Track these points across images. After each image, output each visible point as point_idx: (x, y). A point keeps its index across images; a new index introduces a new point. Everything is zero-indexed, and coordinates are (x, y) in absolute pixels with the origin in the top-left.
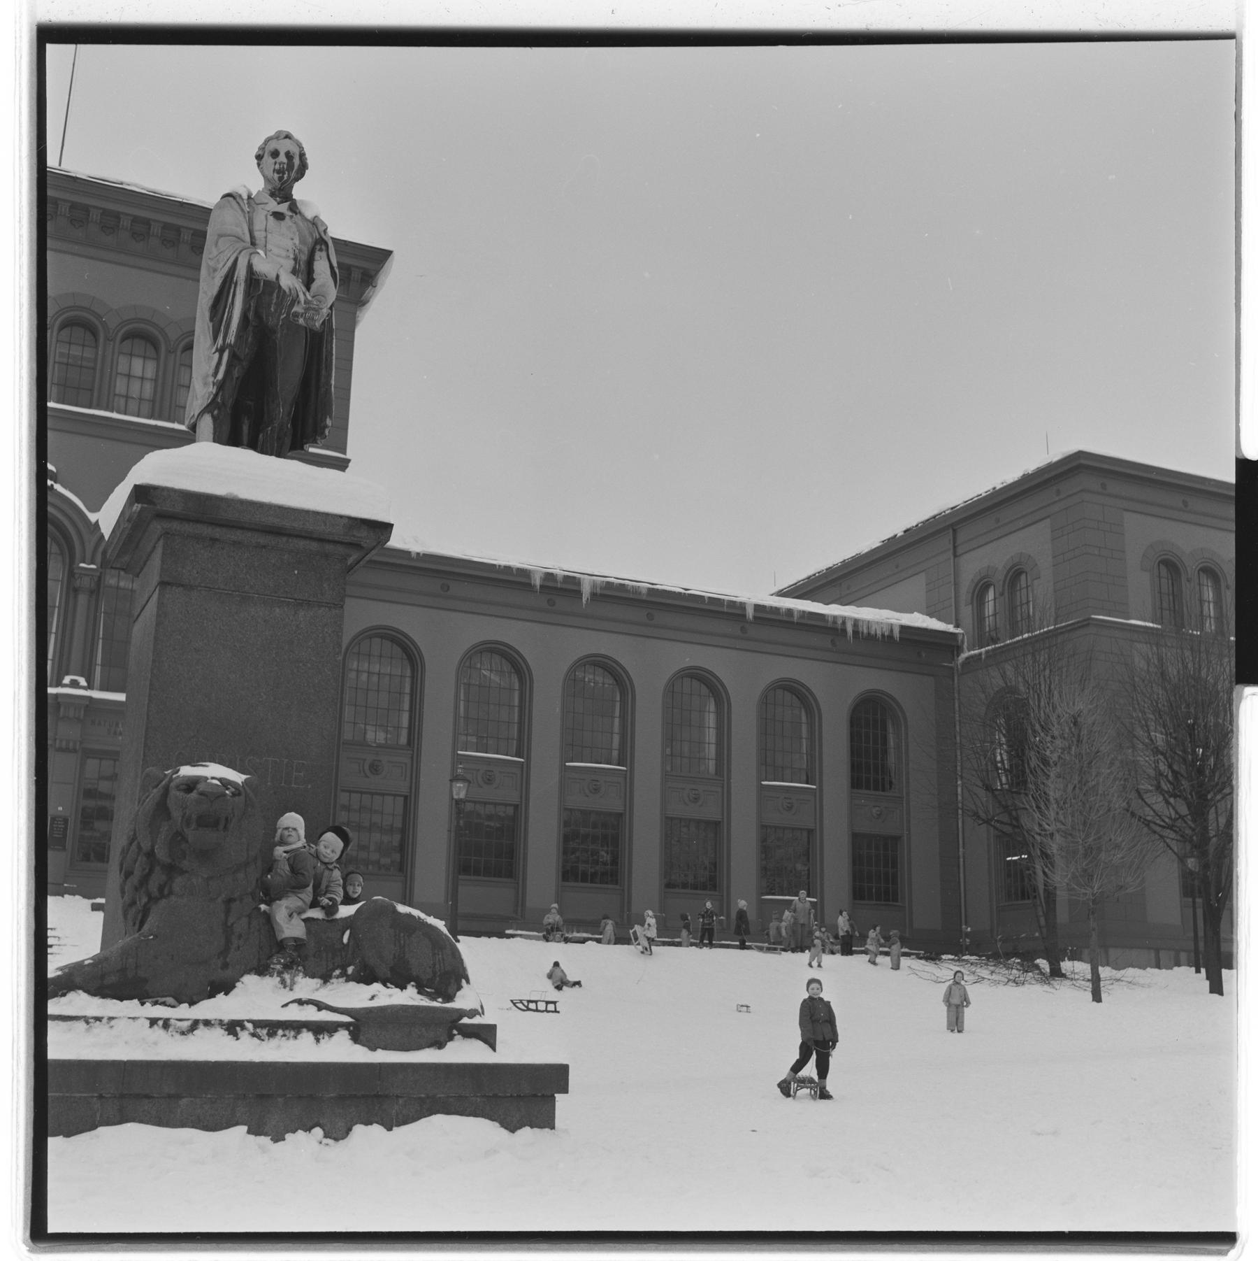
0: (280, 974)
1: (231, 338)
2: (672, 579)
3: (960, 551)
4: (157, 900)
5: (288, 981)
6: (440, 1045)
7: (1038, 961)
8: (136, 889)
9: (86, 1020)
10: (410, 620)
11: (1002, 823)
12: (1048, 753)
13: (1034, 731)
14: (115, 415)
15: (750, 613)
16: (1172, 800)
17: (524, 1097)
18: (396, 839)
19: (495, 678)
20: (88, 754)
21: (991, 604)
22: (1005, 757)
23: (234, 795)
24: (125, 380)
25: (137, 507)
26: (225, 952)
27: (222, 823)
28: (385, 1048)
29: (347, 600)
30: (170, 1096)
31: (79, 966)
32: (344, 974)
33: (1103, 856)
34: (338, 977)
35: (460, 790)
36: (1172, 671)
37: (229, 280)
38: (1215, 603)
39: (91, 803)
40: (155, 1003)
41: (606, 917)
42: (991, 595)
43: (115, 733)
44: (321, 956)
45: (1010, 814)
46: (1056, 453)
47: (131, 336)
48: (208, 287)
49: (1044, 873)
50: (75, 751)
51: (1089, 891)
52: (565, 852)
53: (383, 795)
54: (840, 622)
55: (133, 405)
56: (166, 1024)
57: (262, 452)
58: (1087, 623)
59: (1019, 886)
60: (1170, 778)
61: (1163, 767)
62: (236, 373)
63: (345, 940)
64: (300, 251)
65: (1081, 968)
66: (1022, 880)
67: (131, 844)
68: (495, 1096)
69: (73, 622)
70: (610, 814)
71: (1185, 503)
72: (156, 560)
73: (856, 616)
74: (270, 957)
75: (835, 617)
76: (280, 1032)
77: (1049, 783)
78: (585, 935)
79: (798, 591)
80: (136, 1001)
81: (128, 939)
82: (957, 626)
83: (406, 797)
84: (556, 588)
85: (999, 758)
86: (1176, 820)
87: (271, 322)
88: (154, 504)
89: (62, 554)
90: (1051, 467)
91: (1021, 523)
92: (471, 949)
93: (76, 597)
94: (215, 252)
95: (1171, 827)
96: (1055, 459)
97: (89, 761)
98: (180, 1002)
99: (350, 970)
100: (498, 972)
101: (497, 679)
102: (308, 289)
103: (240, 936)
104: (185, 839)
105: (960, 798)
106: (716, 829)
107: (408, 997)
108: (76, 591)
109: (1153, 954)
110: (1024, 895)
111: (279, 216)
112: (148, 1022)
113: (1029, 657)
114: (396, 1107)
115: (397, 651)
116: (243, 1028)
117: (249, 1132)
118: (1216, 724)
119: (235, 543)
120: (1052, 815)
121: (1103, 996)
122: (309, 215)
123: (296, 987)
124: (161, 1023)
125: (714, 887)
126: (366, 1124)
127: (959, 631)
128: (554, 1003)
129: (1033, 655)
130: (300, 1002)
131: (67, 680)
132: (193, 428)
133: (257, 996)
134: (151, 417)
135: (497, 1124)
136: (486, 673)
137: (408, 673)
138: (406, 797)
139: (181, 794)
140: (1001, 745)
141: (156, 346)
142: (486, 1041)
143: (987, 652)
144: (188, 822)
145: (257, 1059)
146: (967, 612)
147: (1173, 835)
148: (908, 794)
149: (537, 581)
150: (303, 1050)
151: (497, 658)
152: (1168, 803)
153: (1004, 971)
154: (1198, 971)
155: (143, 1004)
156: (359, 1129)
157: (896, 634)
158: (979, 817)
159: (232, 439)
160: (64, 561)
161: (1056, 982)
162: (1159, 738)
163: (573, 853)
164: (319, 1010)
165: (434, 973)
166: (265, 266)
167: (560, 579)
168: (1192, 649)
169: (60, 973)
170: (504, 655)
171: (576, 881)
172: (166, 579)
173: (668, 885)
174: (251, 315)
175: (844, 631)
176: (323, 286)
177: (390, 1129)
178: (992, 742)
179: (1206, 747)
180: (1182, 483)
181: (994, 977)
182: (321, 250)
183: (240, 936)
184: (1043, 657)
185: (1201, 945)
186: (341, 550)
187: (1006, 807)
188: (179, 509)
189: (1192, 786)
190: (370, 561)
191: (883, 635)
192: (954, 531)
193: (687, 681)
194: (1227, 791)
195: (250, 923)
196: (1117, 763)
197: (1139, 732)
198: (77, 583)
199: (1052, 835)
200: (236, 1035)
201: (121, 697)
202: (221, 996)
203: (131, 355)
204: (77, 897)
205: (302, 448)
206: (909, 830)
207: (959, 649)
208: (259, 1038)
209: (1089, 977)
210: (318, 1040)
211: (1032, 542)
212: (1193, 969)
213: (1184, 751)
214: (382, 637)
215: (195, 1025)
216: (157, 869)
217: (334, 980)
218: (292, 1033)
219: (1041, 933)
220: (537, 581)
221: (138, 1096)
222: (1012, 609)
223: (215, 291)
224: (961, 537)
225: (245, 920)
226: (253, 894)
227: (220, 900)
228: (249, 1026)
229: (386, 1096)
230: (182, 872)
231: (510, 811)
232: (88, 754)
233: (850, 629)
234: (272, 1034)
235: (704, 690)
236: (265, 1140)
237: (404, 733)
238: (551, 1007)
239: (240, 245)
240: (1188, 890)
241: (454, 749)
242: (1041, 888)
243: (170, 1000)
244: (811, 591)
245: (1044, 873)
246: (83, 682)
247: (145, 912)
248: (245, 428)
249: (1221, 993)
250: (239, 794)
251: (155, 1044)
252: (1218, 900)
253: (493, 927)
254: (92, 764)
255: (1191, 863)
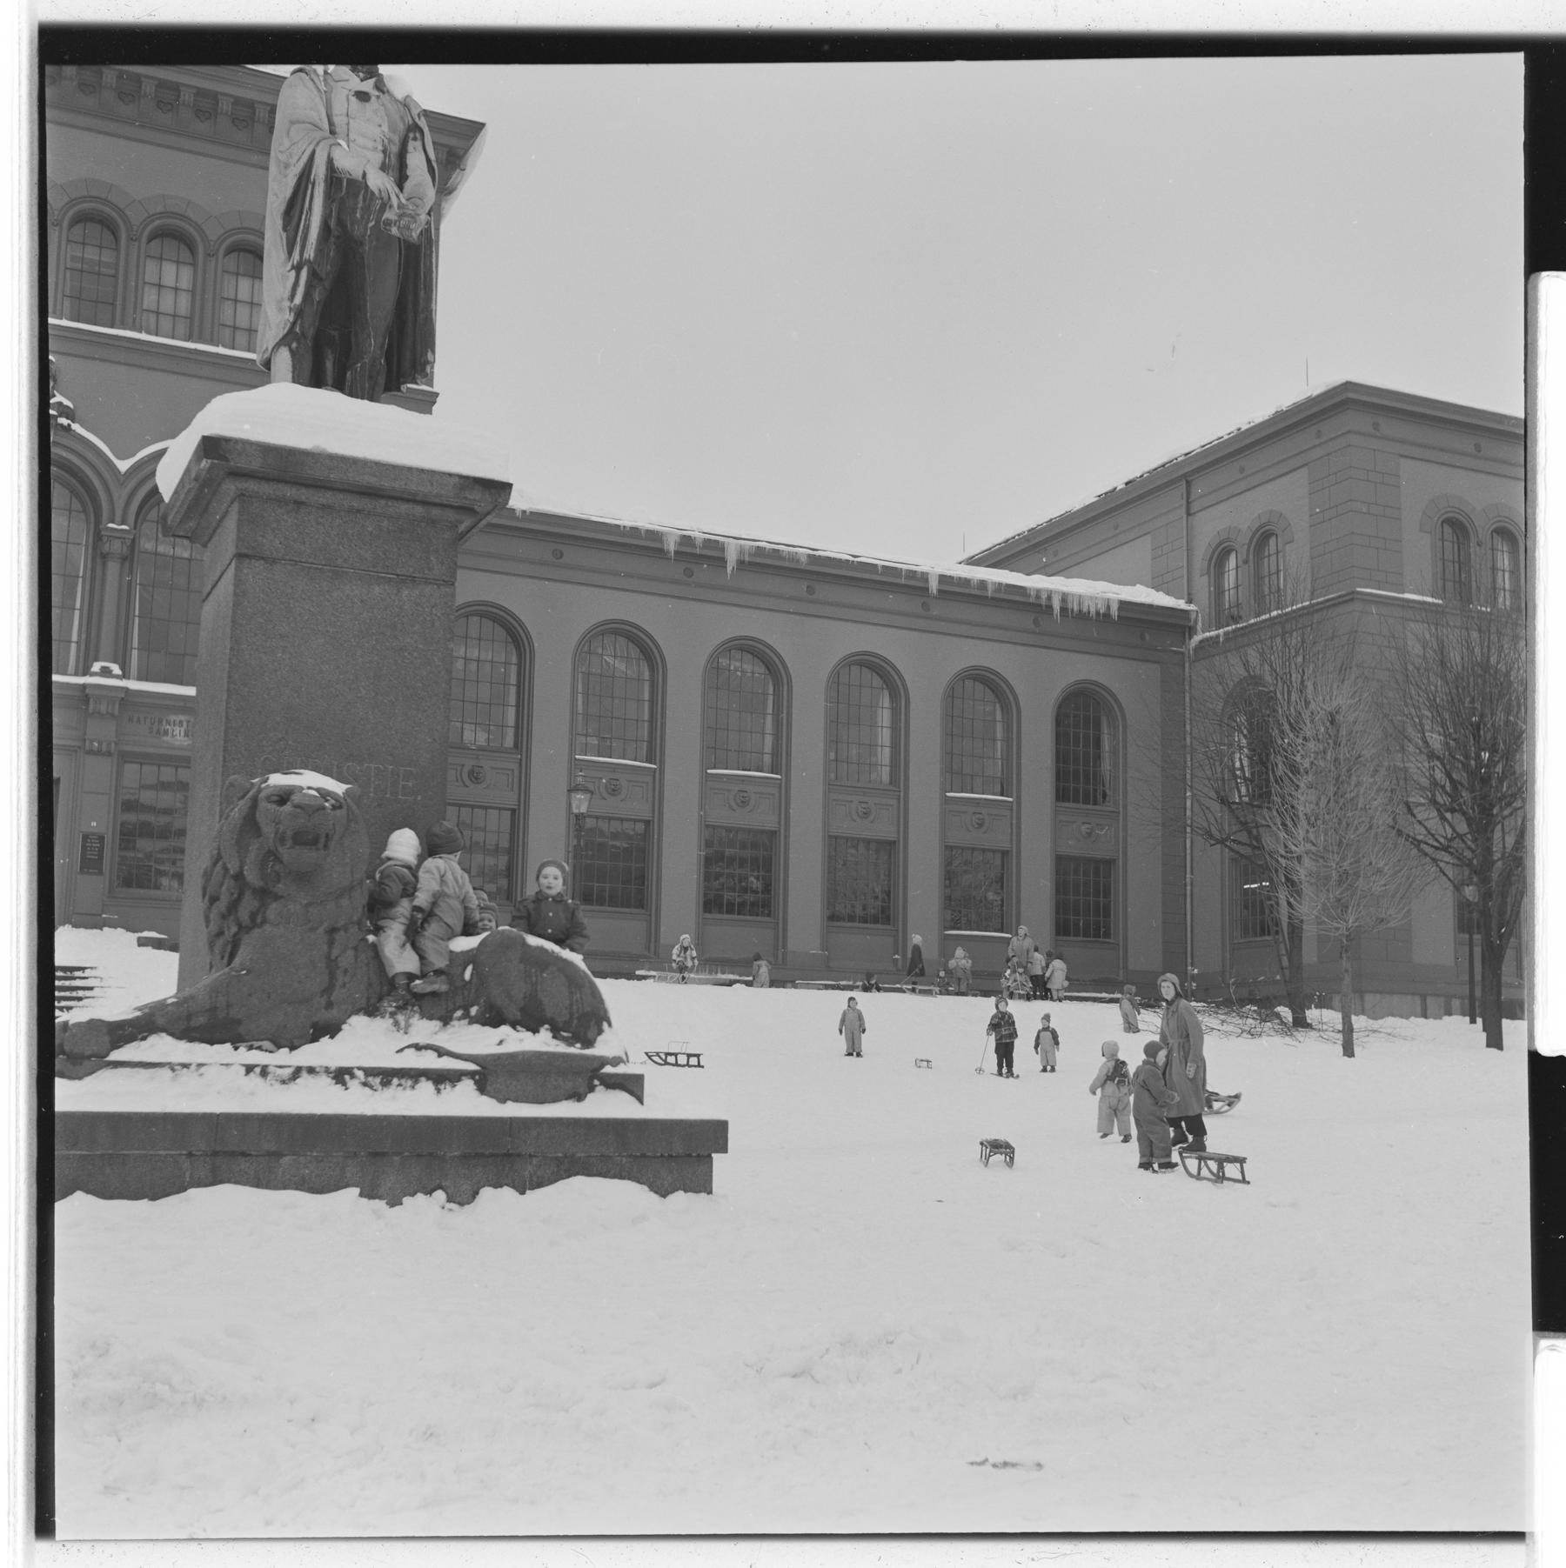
0: (392, 1015)
1: (310, 253)
2: (837, 546)
3: (1195, 507)
4: (248, 929)
5: (403, 1024)
6: (580, 1097)
7: (1279, 1009)
8: (224, 917)
9: (172, 1067)
10: (517, 595)
11: (1239, 843)
12: (1298, 759)
13: (1282, 732)
14: (144, 336)
15: (934, 585)
16: (1448, 815)
17: (678, 1157)
18: (503, 861)
19: (620, 665)
20: (125, 757)
21: (1232, 574)
22: (1245, 763)
23: (334, 808)
24: (154, 290)
25: (205, 463)
26: (328, 990)
27: (322, 840)
28: (516, 1100)
29: (460, 573)
30: (270, 1154)
31: (160, 1006)
32: (466, 1015)
33: (1361, 883)
34: (459, 1019)
35: (581, 803)
36: (1455, 657)
37: (305, 178)
38: (1511, 572)
39: (132, 817)
40: (251, 1048)
41: (758, 958)
42: (1232, 562)
43: (158, 732)
44: (440, 997)
45: (1250, 833)
46: (1317, 385)
47: (162, 234)
48: (279, 189)
49: (1289, 904)
50: (109, 754)
51: (1342, 925)
52: (707, 878)
53: (486, 808)
54: (1044, 596)
55: (166, 323)
56: (264, 1072)
57: (351, 395)
58: (1351, 597)
59: (1257, 920)
60: (1448, 788)
61: (1439, 775)
62: (317, 296)
63: (467, 975)
64: (390, 141)
65: (1332, 1017)
66: (1262, 911)
67: (215, 864)
68: (643, 1156)
69: (102, 596)
70: (763, 832)
71: (1478, 447)
72: (231, 523)
73: (1065, 589)
74: (380, 999)
75: (1038, 591)
76: (395, 1081)
77: (1297, 794)
78: (732, 977)
79: (997, 557)
80: (228, 1046)
81: (215, 975)
82: (1190, 602)
83: (513, 811)
84: (694, 555)
85: (1238, 764)
86: (1450, 840)
87: (357, 231)
88: (227, 460)
89: (85, 511)
90: (1311, 402)
91: (1272, 473)
92: (610, 990)
93: (104, 565)
94: (287, 143)
95: (1445, 849)
96: (1316, 393)
97: (128, 767)
98: (279, 1047)
99: (474, 1011)
100: (643, 1016)
101: (623, 667)
102: (401, 189)
103: (346, 971)
104: (278, 859)
105: (1188, 813)
106: (890, 850)
107: (542, 1042)
108: (104, 557)
109: (1418, 1000)
110: (1264, 930)
111: (362, 96)
112: (243, 1070)
113: (1278, 640)
114: (530, 1168)
115: (500, 632)
116: (353, 1076)
117: (361, 1195)
118: (1507, 722)
119: (324, 507)
120: (1301, 833)
121: (1357, 1050)
122: (399, 94)
123: (412, 1030)
124: (258, 1070)
125: (887, 920)
126: (496, 1187)
127: (1192, 607)
128: (698, 1056)
129: (1283, 639)
130: (418, 1047)
131: (96, 667)
132: (268, 364)
133: (366, 1040)
134: (189, 339)
135: (645, 1188)
136: (610, 660)
137: (514, 660)
138: (513, 811)
139: (273, 807)
140: (1241, 748)
141: (192, 249)
142: (632, 1093)
143: (1226, 634)
144: (282, 840)
145: (369, 1112)
146: (1202, 584)
147: (1448, 858)
148: (1125, 808)
149: (671, 547)
150: (421, 1102)
151: (622, 641)
152: (1443, 818)
153: (1238, 1021)
154: (1473, 1021)
155: (236, 1049)
156: (487, 1192)
157: (1114, 611)
158: (1211, 836)
159: (316, 380)
160: (87, 521)
161: (1300, 1034)
162: (1436, 740)
163: (717, 879)
164: (440, 1055)
165: (571, 1015)
166: (350, 161)
167: (699, 543)
168: (1480, 631)
169: (139, 1013)
170: (631, 638)
171: (720, 912)
172: (245, 551)
173: (832, 918)
174: (332, 223)
175: (1050, 607)
176: (419, 185)
177: (523, 1193)
178: (1230, 745)
179: (1493, 750)
180: (1474, 421)
181: (1225, 1027)
182: (415, 139)
183: (346, 971)
184: (1294, 640)
185: (1478, 992)
186: (451, 515)
187: (1244, 824)
188: (256, 464)
189: (1474, 798)
190: (490, 525)
191: (1098, 613)
192: (1188, 482)
193: (855, 669)
194: (1518, 804)
195: (356, 957)
196: (1383, 771)
197: (1411, 731)
198: (106, 548)
199: (1299, 859)
200: (344, 1084)
201: (190, 691)
202: (326, 1040)
203: (161, 259)
204: (120, 930)
205: (399, 390)
206: (1125, 853)
207: (1192, 631)
208: (371, 1087)
209: (1340, 1027)
210: (439, 1091)
211: (1284, 496)
212: (1467, 1019)
213: (1467, 757)
214: (482, 615)
215: (297, 1072)
216: (248, 895)
217: (455, 1023)
218: (409, 1083)
219: (1283, 975)
220: (671, 547)
221: (233, 1154)
222: (1258, 579)
223: (288, 193)
224: (1198, 490)
225: (350, 953)
226: (359, 923)
227: (321, 930)
228: (360, 1074)
229: (519, 1155)
230: (277, 897)
231: (640, 827)
232: (125, 757)
233: (1056, 605)
234: (386, 1084)
235: (877, 681)
236: (380, 1204)
237: (510, 733)
238: (693, 1061)
239: (318, 135)
240: (1464, 925)
241: (572, 752)
242: (1285, 920)
243: (267, 1044)
244: (1013, 556)
245: (1289, 904)
246: (116, 669)
247: (235, 945)
248: (329, 365)
249: (1500, 1047)
250: (340, 807)
251: (253, 1094)
252: (1501, 937)
253: (624, 971)
254: (131, 770)
255: (1470, 892)
